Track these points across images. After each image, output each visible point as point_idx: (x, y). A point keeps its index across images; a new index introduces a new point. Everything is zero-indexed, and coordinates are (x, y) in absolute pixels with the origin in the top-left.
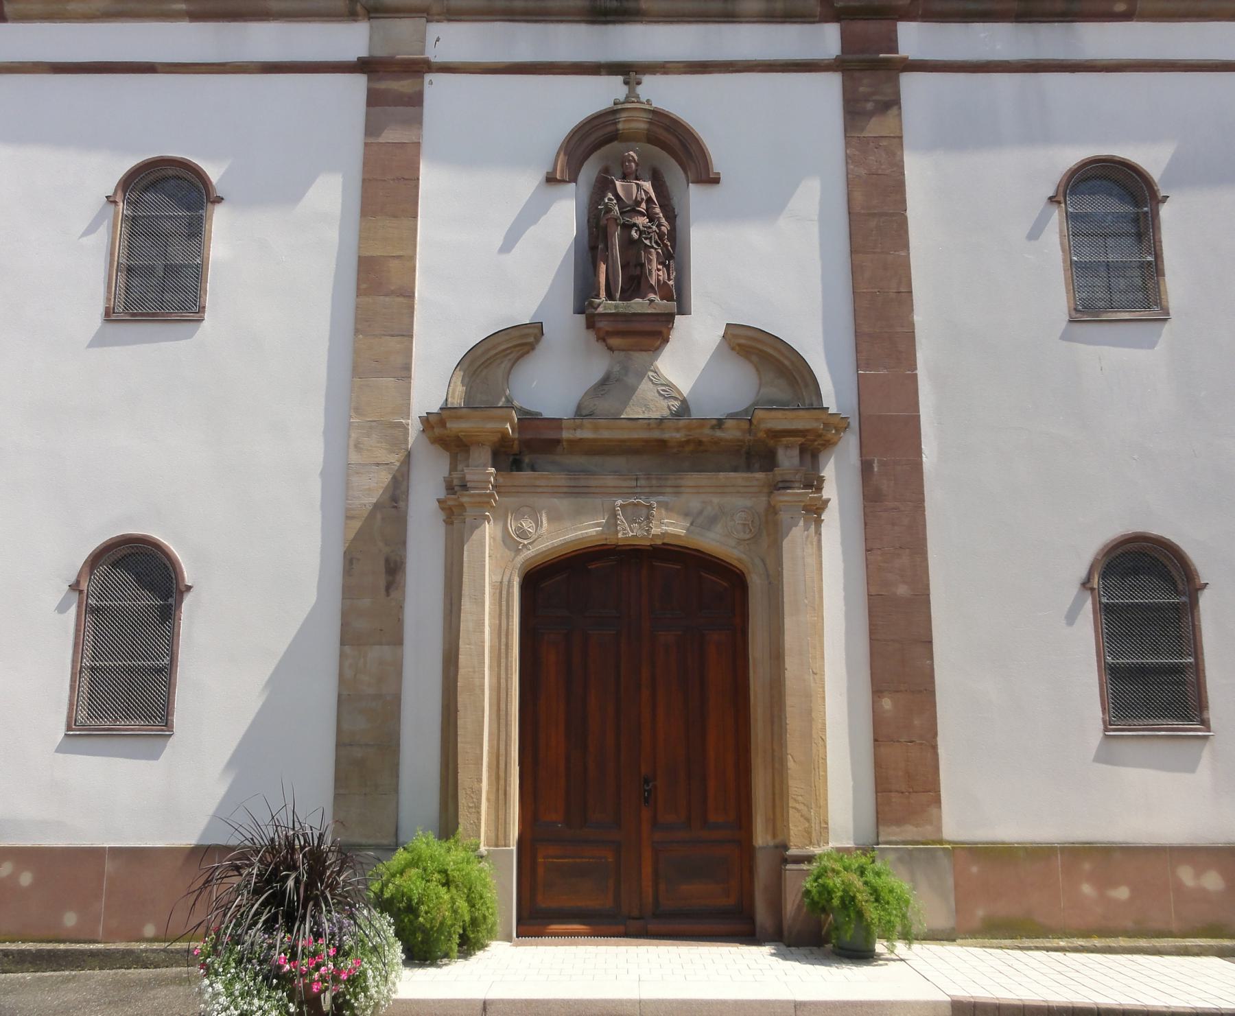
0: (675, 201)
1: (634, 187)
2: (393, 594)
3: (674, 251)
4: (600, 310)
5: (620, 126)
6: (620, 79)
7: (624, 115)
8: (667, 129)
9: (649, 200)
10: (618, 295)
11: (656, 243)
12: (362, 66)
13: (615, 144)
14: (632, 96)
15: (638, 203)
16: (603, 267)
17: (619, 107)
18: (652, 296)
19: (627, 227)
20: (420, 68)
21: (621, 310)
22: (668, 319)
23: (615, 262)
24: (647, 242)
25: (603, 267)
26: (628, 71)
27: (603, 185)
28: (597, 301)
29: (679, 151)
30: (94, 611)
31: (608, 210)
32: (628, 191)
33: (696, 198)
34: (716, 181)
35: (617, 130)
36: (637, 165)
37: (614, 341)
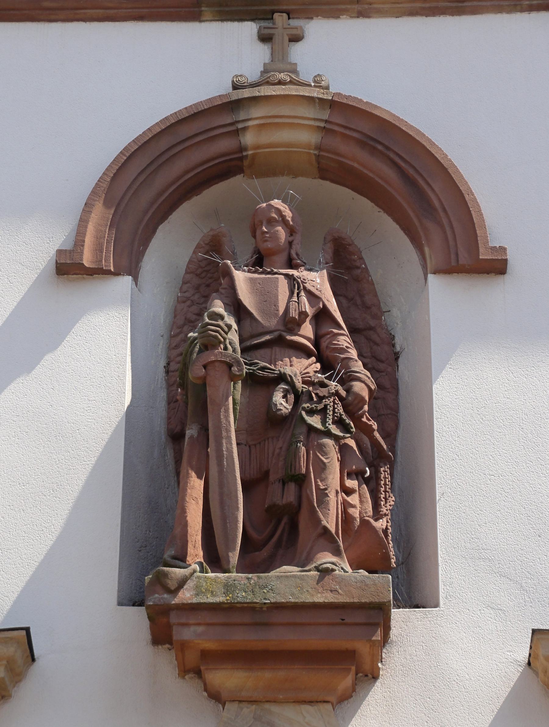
0: (396, 318)
1: (283, 283)
3: (387, 439)
4: (186, 595)
5: (249, 139)
7: (257, 112)
8: (367, 143)
9: (322, 316)
10: (234, 557)
11: (339, 422)
13: (238, 180)
14: (278, 70)
15: (292, 324)
16: (196, 486)
17: (246, 93)
18: (326, 558)
19: (262, 383)
21: (242, 596)
22: (374, 618)
23: (224, 474)
24: (315, 421)
25: (196, 486)
27: (206, 277)
28: (178, 572)
29: (401, 188)
31: (209, 344)
32: (266, 297)
33: (441, 311)
34: (497, 267)
35: (242, 149)
36: (291, 231)
37: (226, 678)
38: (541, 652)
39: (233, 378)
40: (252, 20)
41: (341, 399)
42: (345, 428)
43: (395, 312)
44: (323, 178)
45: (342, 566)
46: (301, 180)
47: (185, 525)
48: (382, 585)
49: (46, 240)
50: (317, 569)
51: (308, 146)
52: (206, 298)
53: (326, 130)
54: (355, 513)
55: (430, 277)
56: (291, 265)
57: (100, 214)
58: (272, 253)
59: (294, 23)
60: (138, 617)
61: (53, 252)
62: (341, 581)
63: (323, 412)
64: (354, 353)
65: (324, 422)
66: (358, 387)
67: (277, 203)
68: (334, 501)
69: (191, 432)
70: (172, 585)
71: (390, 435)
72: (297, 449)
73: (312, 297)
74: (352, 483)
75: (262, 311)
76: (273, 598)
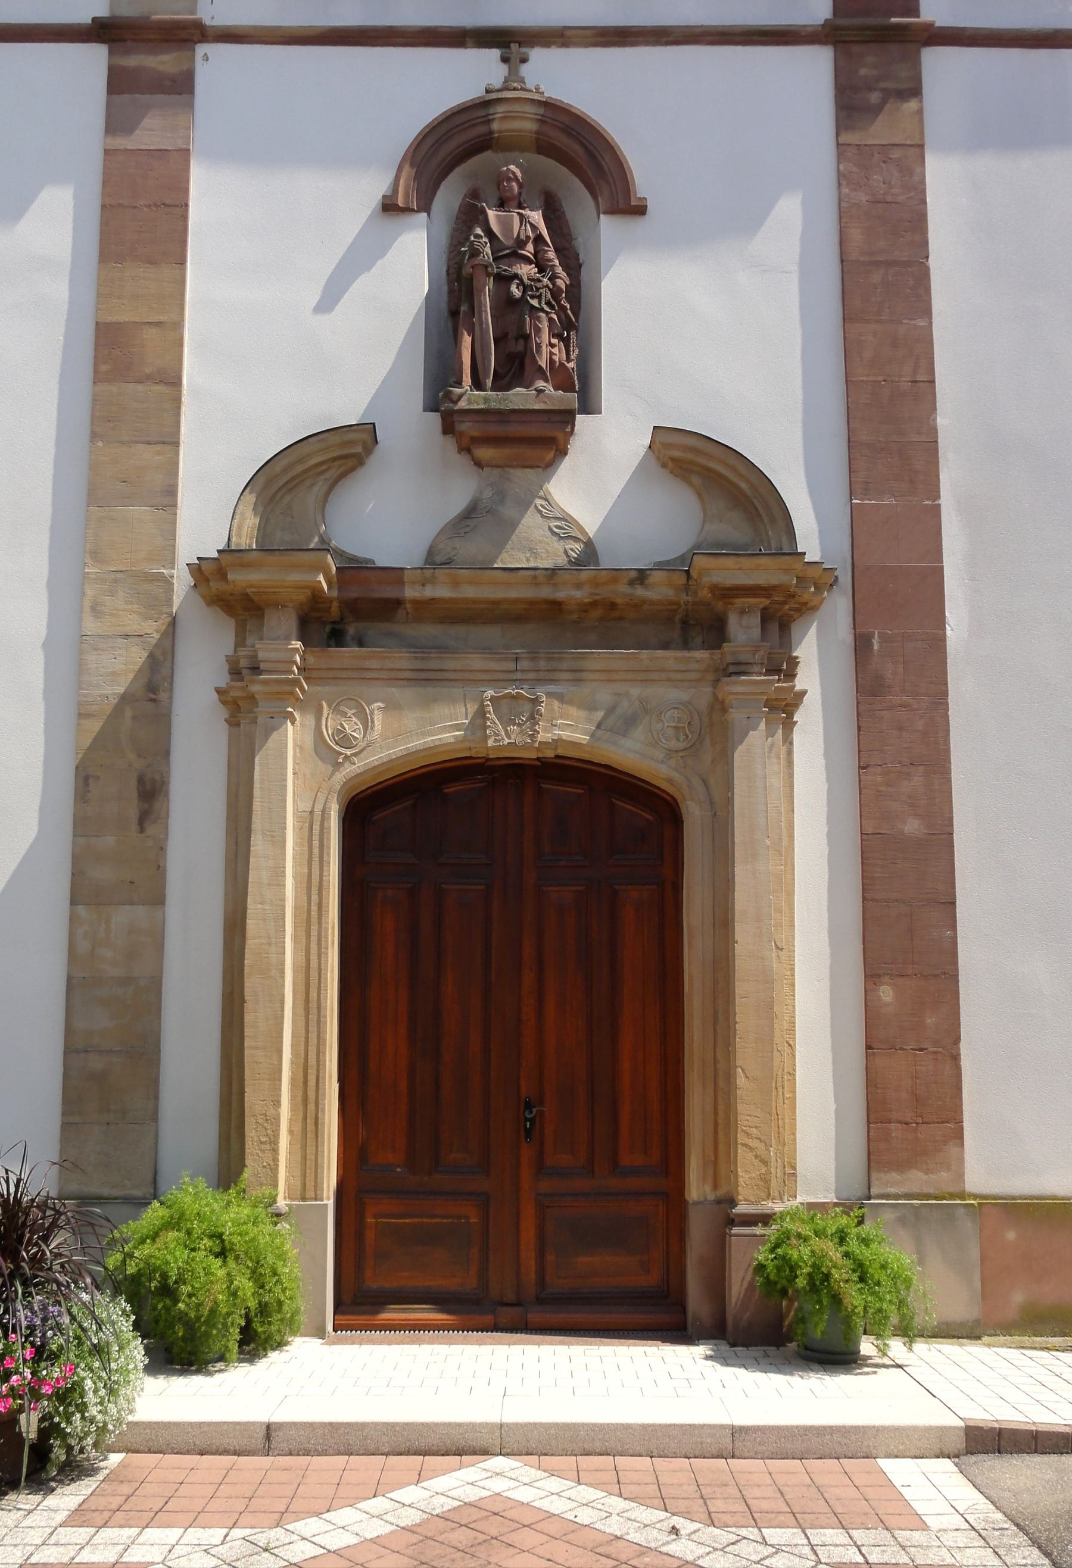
1: (516, 219)
4: (463, 404)
5: (495, 126)
7: (501, 109)
8: (567, 130)
9: (539, 239)
10: (489, 382)
11: (548, 303)
13: (488, 155)
14: (513, 80)
15: (521, 243)
16: (467, 340)
17: (494, 96)
18: (540, 384)
19: (504, 280)
21: (494, 405)
22: (566, 418)
24: (535, 302)
25: (467, 340)
27: (470, 215)
29: (583, 162)
31: (475, 253)
32: (506, 226)
34: (640, 210)
35: (491, 132)
36: (521, 186)
37: (484, 453)
38: (657, 440)
39: (488, 275)
40: (497, 47)
41: (550, 290)
42: (552, 307)
43: (580, 239)
44: (539, 153)
45: (549, 389)
46: (526, 154)
47: (462, 363)
48: (572, 399)
49: (376, 184)
50: (536, 390)
51: (530, 132)
52: (470, 229)
53: (542, 122)
54: (556, 358)
55: (602, 216)
56: (520, 207)
57: (408, 172)
58: (510, 199)
59: (523, 50)
60: (435, 418)
61: (380, 197)
62: (549, 396)
63: (539, 297)
64: (557, 262)
65: (540, 303)
66: (559, 282)
67: (512, 167)
68: (545, 349)
69: (463, 308)
70: (455, 398)
71: (576, 314)
72: (525, 319)
73: (534, 227)
74: (554, 341)
75: (504, 235)
76: (511, 407)
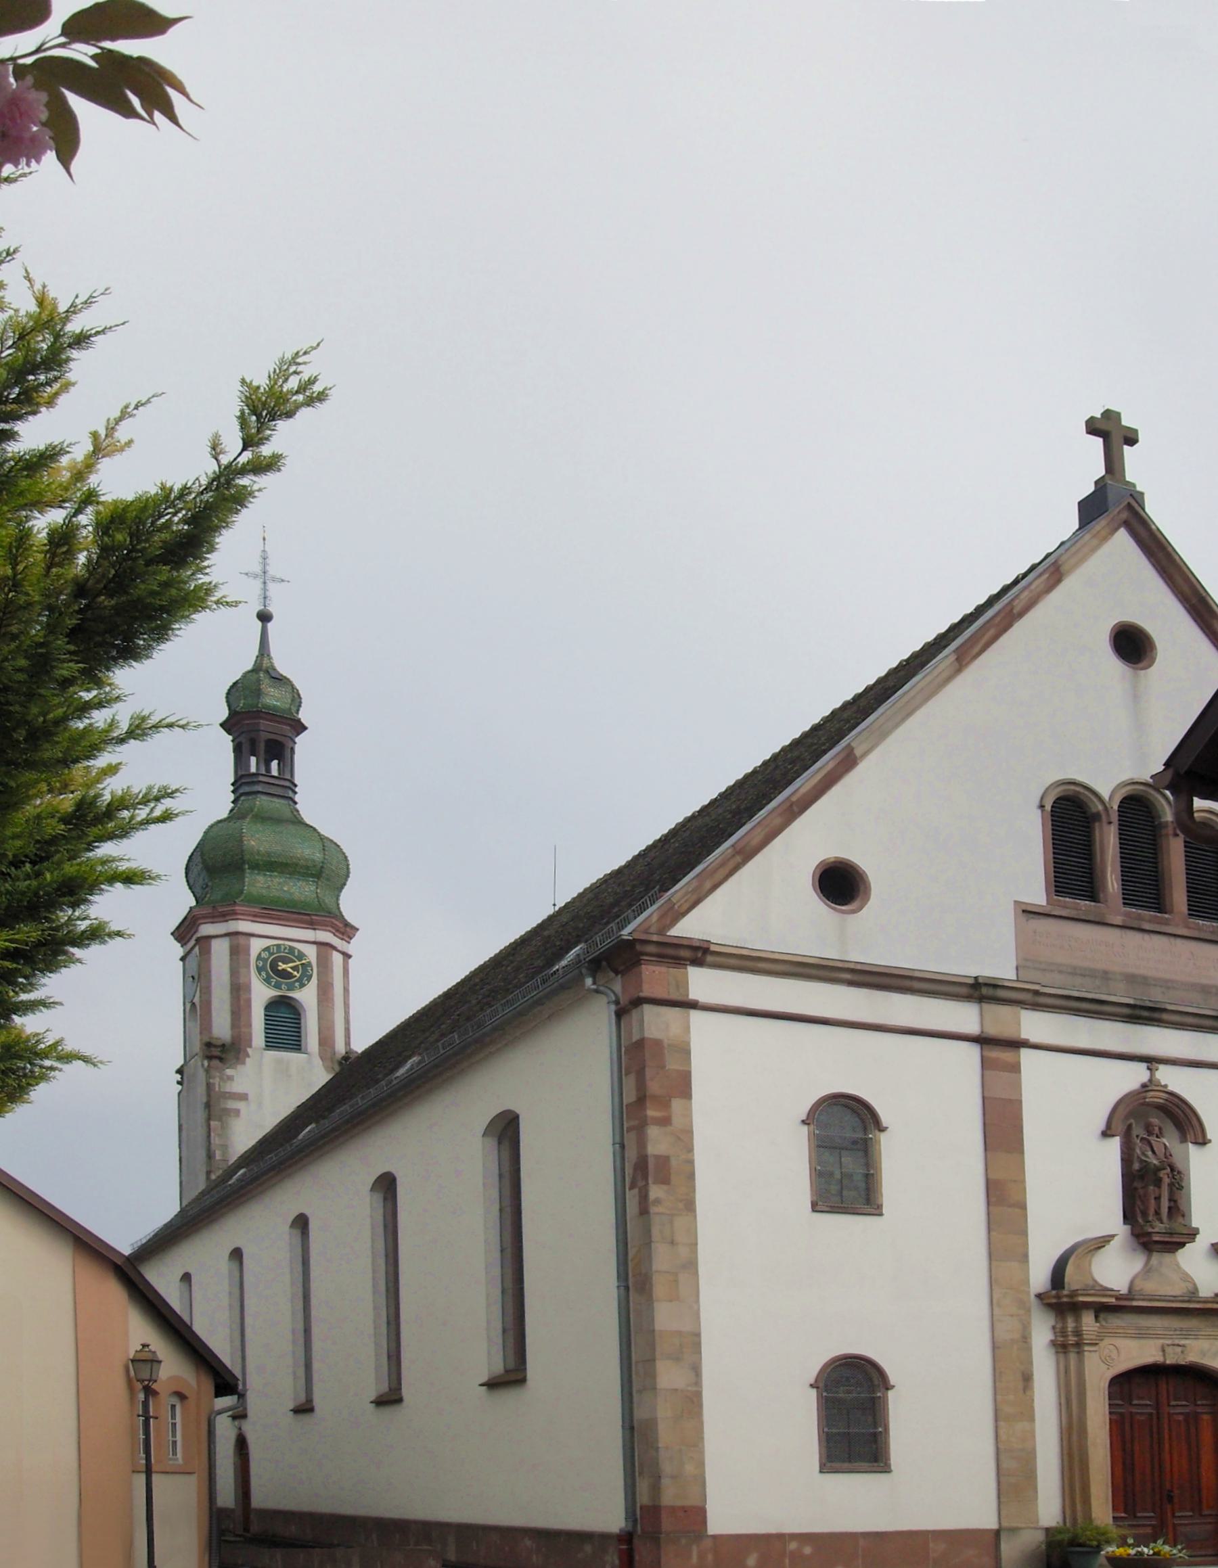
2: (1028, 1393)
6: (1144, 1065)
12: (981, 1040)
20: (1017, 1044)
26: (1151, 1061)
29: (1183, 1119)
30: (827, 1399)
